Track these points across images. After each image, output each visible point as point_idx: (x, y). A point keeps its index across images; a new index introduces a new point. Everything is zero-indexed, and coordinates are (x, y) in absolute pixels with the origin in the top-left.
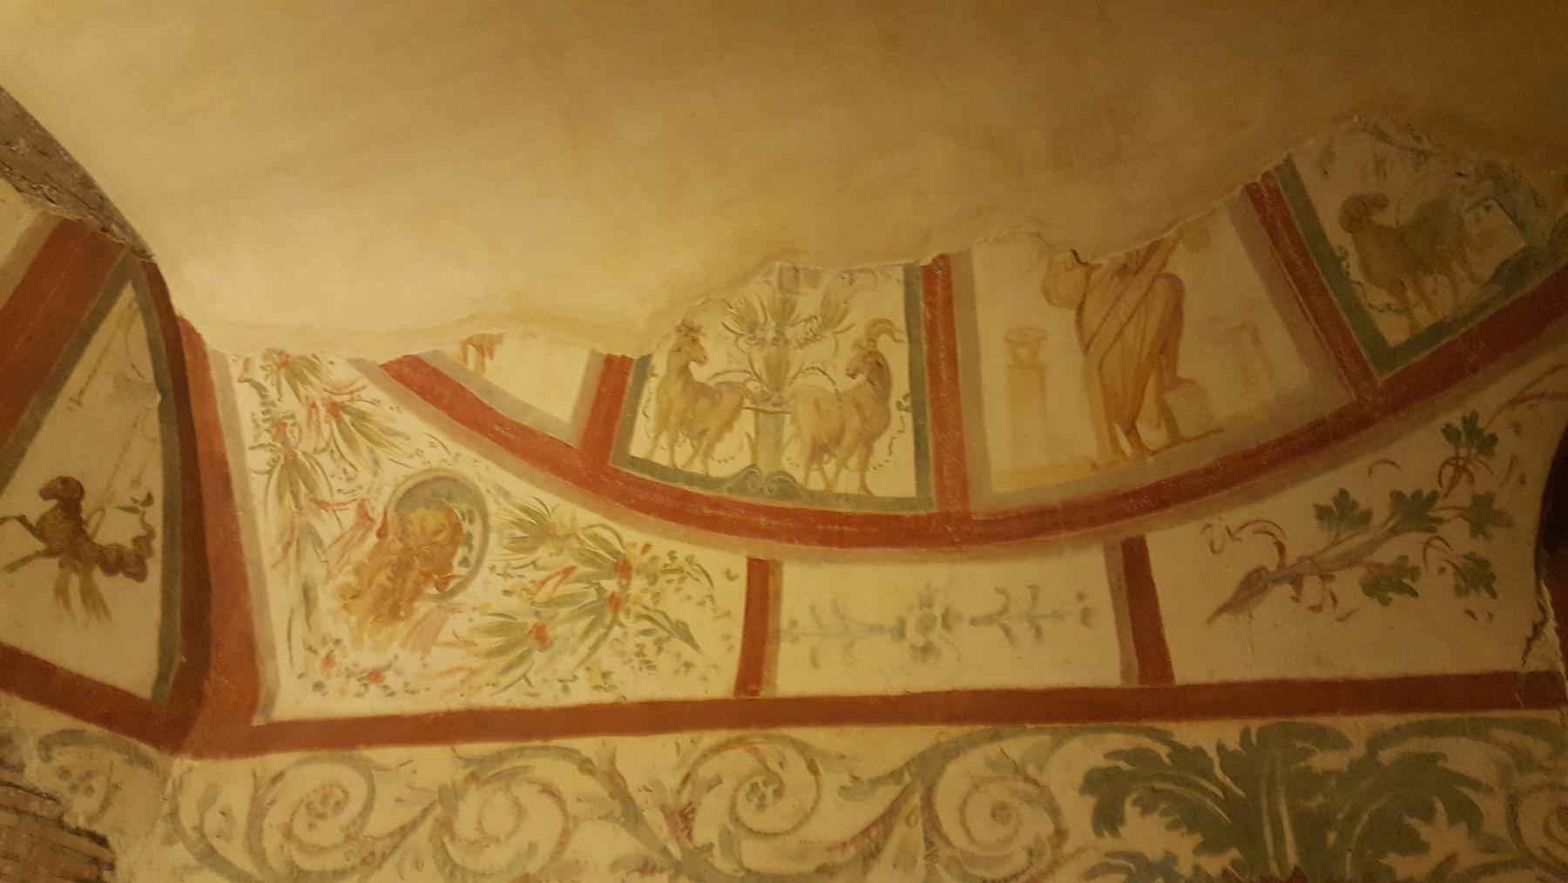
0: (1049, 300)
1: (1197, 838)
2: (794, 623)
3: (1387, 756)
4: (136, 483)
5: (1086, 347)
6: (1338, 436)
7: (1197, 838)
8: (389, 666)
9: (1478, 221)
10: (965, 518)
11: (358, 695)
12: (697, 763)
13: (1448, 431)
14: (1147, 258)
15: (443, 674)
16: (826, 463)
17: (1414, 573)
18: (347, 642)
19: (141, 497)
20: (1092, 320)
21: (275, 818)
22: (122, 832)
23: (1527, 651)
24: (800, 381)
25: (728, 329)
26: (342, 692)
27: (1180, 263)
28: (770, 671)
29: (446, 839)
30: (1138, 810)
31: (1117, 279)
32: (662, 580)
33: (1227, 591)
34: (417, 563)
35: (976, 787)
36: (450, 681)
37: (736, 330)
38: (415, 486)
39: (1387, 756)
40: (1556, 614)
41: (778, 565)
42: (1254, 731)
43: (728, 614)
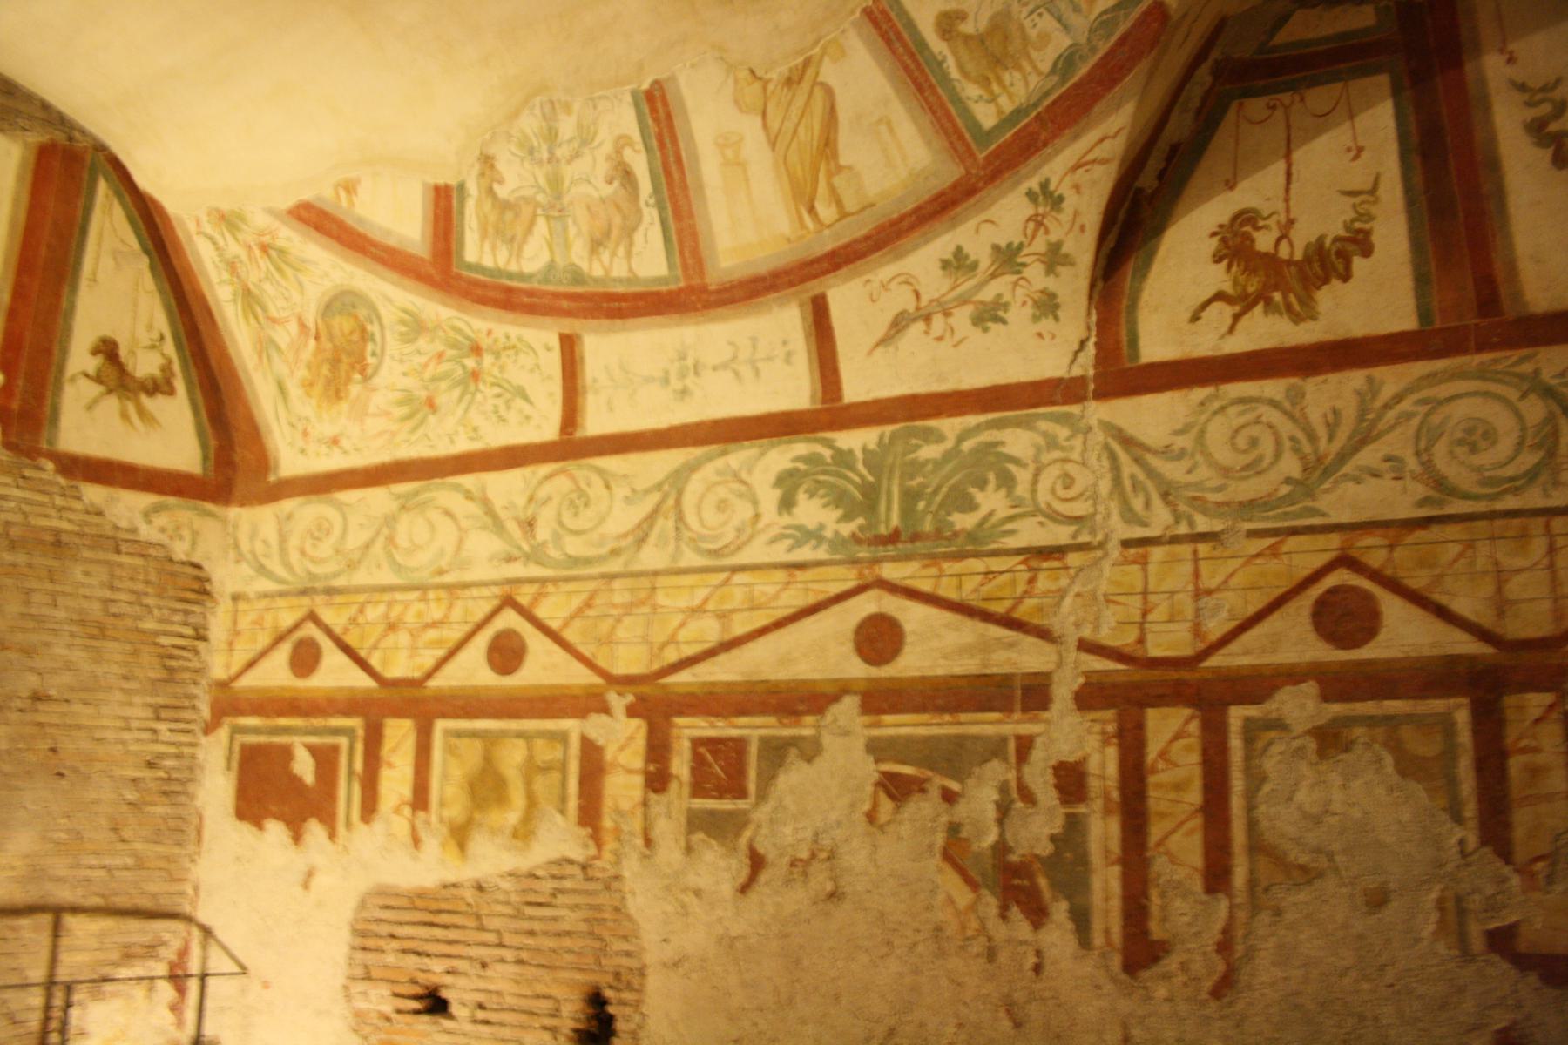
1: (839, 513)
2: (595, 380)
4: (150, 327)
5: (773, 144)
6: (954, 203)
7: (839, 513)
9: (1035, 25)
10: (703, 289)
13: (1031, 195)
14: (804, 71)
17: (1006, 306)
19: (155, 336)
20: (774, 124)
21: (294, 542)
22: (209, 559)
23: (1073, 361)
27: (829, 73)
30: (807, 495)
31: (785, 90)
32: (503, 354)
33: (880, 331)
35: (708, 489)
39: (967, 446)
40: (1098, 331)
41: (579, 337)
42: (887, 435)
43: (550, 378)
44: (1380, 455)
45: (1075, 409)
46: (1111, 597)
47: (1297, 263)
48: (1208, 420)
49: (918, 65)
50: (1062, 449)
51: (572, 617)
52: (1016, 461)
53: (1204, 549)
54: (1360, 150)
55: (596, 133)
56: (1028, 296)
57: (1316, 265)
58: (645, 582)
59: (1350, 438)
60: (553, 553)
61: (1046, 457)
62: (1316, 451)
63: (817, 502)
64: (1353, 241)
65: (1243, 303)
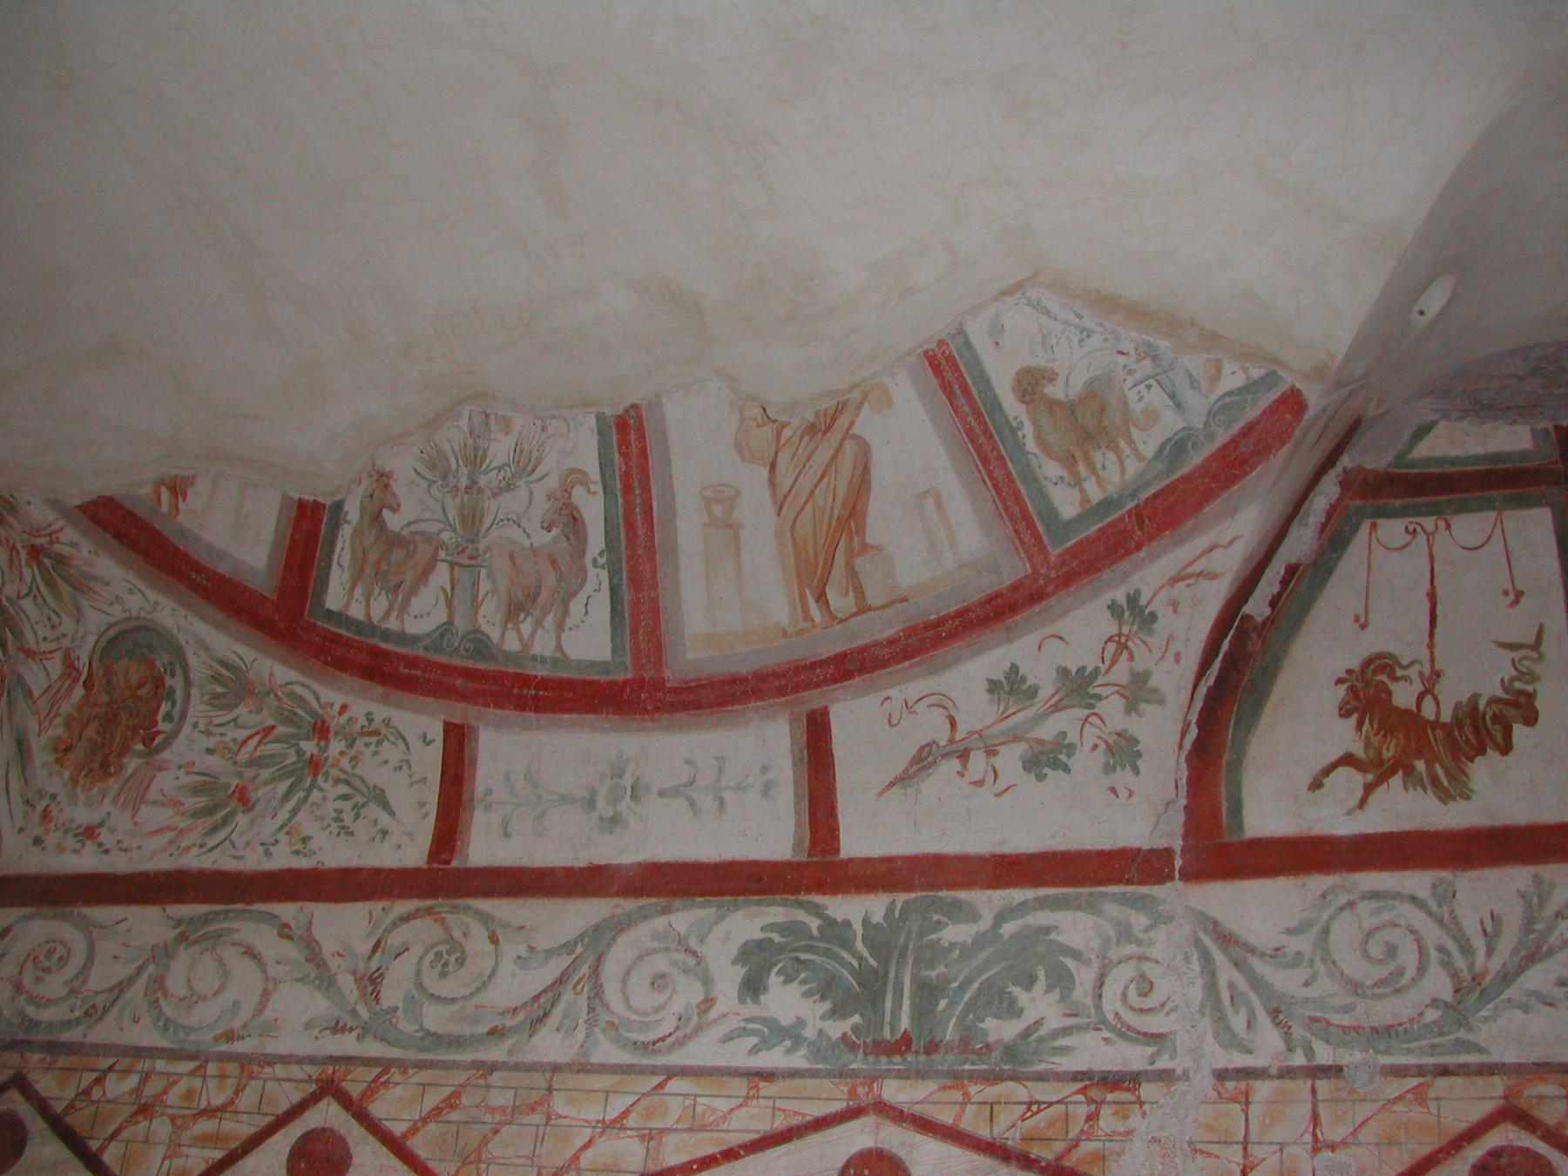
0: (743, 459)
1: (827, 1005)
3: (1008, 929)
6: (1014, 609)
7: (827, 1005)
8: (102, 824)
9: (1142, 398)
10: (658, 685)
11: (75, 851)
12: (387, 931)
13: (1113, 607)
14: (834, 419)
15: (153, 833)
16: (522, 622)
17: (1070, 749)
18: (61, 798)
24: (495, 533)
25: (419, 474)
26: (61, 849)
28: (463, 840)
29: (159, 994)
32: (360, 743)
34: (124, 717)
35: (640, 958)
36: (160, 841)
37: (428, 476)
38: (116, 637)
39: (1008, 929)
41: (474, 730)
44: (1553, 977)
45: (1157, 891)
46: (1199, 1146)
47: (1444, 726)
48: (1331, 918)
49: (986, 429)
50: (1139, 943)
51: (425, 1120)
52: (1076, 955)
53: (1322, 1085)
54: (1519, 595)
55: (539, 461)
56: (1099, 737)
57: (1468, 731)
58: (539, 1080)
59: (1515, 952)
60: (405, 1025)
61: (1115, 953)
62: (1471, 966)
63: (795, 989)
64: (1514, 704)
65: (1378, 771)
